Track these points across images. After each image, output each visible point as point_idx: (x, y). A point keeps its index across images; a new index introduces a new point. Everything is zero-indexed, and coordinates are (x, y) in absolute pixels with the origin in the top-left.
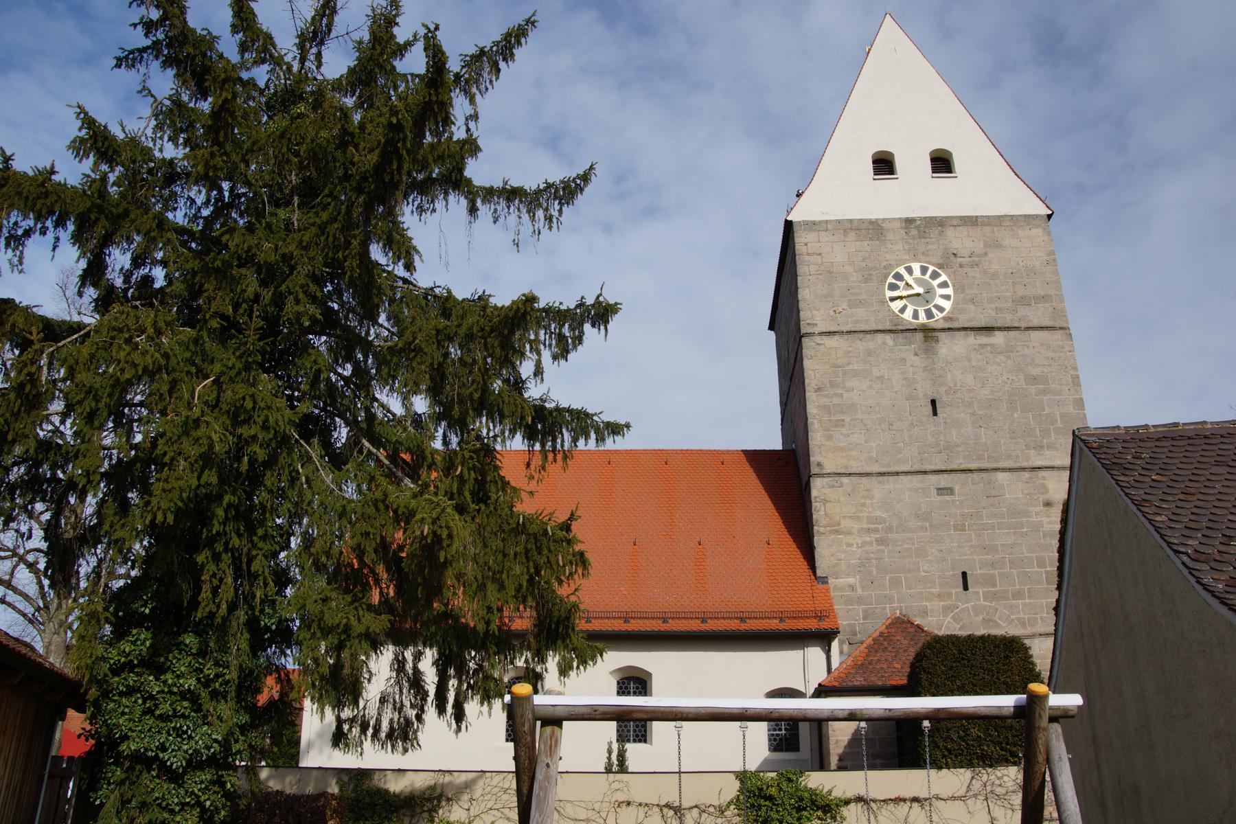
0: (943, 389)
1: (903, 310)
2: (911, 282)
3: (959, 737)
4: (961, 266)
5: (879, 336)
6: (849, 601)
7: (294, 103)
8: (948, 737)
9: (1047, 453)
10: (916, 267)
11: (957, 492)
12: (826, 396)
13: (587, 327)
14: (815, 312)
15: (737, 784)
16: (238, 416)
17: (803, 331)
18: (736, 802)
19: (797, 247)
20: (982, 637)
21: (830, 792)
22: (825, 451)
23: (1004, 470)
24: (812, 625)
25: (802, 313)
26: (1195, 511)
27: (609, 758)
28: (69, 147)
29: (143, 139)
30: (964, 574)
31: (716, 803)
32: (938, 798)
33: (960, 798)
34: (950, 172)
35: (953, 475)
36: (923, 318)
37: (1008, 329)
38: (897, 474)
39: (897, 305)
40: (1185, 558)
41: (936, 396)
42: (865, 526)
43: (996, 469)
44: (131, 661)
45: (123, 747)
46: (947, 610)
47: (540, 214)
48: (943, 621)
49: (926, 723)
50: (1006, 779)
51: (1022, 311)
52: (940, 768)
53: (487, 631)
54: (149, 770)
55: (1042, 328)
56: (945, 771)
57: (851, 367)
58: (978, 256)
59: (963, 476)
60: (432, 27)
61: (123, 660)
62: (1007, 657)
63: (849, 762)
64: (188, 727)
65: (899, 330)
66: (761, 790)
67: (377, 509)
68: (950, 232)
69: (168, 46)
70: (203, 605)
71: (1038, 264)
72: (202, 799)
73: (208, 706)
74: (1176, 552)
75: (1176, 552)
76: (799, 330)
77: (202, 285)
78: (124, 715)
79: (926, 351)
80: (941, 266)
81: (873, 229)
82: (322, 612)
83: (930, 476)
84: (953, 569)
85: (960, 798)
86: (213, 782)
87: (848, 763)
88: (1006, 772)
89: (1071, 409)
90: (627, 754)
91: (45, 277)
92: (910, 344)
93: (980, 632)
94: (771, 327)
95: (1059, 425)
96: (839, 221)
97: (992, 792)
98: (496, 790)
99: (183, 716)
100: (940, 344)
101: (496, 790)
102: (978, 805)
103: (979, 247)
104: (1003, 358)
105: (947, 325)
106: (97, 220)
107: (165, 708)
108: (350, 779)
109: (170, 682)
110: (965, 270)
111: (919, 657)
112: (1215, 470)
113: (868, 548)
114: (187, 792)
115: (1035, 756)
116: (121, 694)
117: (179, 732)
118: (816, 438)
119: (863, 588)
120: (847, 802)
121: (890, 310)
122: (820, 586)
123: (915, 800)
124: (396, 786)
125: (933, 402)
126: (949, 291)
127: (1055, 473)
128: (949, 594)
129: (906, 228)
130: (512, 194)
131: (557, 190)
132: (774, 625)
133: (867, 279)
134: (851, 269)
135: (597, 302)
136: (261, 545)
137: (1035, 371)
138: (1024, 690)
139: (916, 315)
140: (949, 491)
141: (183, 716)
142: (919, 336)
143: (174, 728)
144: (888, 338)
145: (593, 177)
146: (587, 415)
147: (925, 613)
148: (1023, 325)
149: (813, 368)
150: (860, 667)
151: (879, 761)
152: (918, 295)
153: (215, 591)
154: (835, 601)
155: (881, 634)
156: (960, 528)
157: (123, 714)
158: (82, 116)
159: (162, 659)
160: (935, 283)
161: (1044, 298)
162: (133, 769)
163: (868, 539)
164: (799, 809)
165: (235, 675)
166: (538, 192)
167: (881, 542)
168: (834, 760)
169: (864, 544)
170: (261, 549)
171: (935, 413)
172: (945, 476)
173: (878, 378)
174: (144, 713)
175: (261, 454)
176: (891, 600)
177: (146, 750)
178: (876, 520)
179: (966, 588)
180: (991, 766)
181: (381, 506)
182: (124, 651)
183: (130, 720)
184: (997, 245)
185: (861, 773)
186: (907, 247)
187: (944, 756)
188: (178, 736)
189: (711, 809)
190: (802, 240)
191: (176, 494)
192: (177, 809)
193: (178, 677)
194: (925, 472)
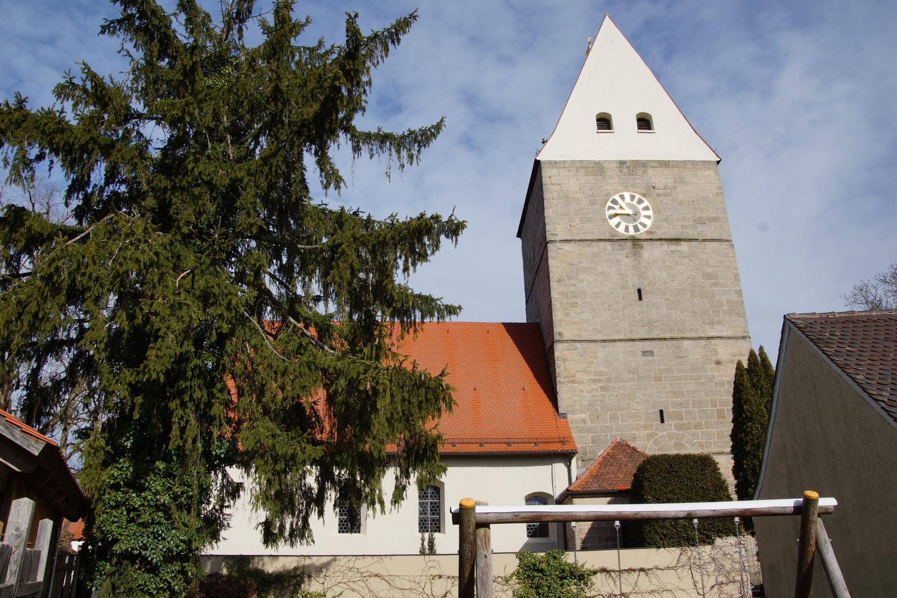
0: (646, 282)
1: (618, 225)
2: (623, 205)
3: (672, 526)
4: (658, 195)
5: (602, 244)
6: (582, 430)
7: (224, 65)
8: (664, 526)
9: (718, 327)
10: (627, 195)
11: (656, 353)
12: (565, 285)
13: (442, 237)
14: (556, 224)
15: (518, 561)
16: (206, 299)
17: (548, 239)
18: (517, 574)
19: (544, 179)
20: (685, 456)
21: (583, 565)
22: (564, 324)
23: (688, 339)
24: (558, 448)
25: (547, 227)
26: (881, 372)
27: (423, 544)
28: (54, 91)
29: (125, 89)
30: (661, 412)
31: (503, 575)
32: (657, 568)
33: (672, 568)
34: (650, 129)
35: (653, 342)
36: (632, 232)
37: (691, 240)
38: (615, 341)
39: (613, 222)
40: (883, 405)
41: (641, 287)
42: (593, 377)
43: (683, 338)
44: (118, 483)
45: (116, 548)
46: (649, 436)
47: (404, 153)
48: (654, 443)
49: (696, 521)
50: (703, 554)
51: (700, 228)
52: (659, 547)
53: (380, 457)
54: (133, 563)
55: (713, 240)
56: (662, 549)
57: (582, 265)
58: (670, 188)
59: (660, 342)
60: (353, 15)
61: (112, 482)
62: (703, 470)
63: (587, 546)
64: (163, 532)
65: (615, 240)
66: (534, 565)
67: (310, 369)
68: (650, 171)
69: (140, 18)
70: (173, 440)
71: (710, 195)
72: (173, 584)
73: (176, 515)
74: (876, 400)
75: (876, 400)
76: (545, 237)
77: (171, 200)
78: (111, 522)
79: (635, 254)
80: (644, 195)
81: (597, 168)
82: (274, 445)
83: (637, 343)
84: (654, 408)
85: (672, 568)
86: (179, 572)
87: (588, 545)
88: (703, 549)
89: (733, 297)
90: (435, 541)
91: (49, 193)
92: (623, 249)
93: (673, 452)
94: (519, 235)
95: (725, 308)
96: (573, 162)
97: (694, 563)
98: (344, 569)
99: (159, 523)
100: (644, 250)
101: (344, 569)
102: (685, 573)
103: (671, 182)
104: (686, 260)
105: (648, 237)
106: (93, 149)
107: (146, 518)
108: (234, 563)
109: (149, 498)
110: (661, 198)
111: (641, 470)
112: (886, 344)
113: (595, 393)
114: (161, 579)
115: (809, 541)
116: (112, 507)
117: (156, 536)
118: (558, 315)
119: (591, 421)
120: (595, 573)
121: (609, 225)
122: (562, 420)
123: (642, 570)
124: (271, 568)
125: (639, 291)
126: (650, 213)
127: (723, 341)
128: (652, 425)
129: (620, 167)
130: (384, 139)
131: (416, 137)
132: (531, 448)
133: (593, 203)
134: (580, 195)
135: (450, 221)
136: (219, 395)
137: (709, 270)
138: (801, 495)
139: (627, 229)
140: (651, 353)
141: (159, 523)
142: (629, 244)
143: (152, 533)
144: (608, 245)
145: (443, 128)
146: (433, 300)
147: (635, 439)
148: (701, 238)
149: (556, 265)
150: (596, 476)
151: (610, 543)
152: (628, 215)
153: (183, 430)
154: (572, 430)
155: (608, 454)
156: (658, 379)
157: (114, 522)
158: (86, 71)
159: (143, 481)
160: (640, 207)
161: (715, 219)
162: (121, 564)
163: (595, 387)
164: (562, 578)
165: (196, 491)
166: (403, 137)
167: (604, 389)
168: (578, 544)
169: (592, 390)
170: (218, 398)
171: (640, 298)
172: (648, 342)
173: (600, 273)
174: (128, 522)
175: (226, 328)
176: (611, 430)
177: (132, 549)
178: (597, 373)
179: (662, 421)
180: (693, 546)
181: (313, 367)
182: (113, 475)
183: (119, 527)
184: (682, 181)
185: (615, 552)
186: (621, 181)
187: (661, 539)
188: (155, 538)
189: (500, 580)
190: (547, 174)
191: (166, 360)
192: (155, 592)
193: (155, 494)
194: (634, 340)
